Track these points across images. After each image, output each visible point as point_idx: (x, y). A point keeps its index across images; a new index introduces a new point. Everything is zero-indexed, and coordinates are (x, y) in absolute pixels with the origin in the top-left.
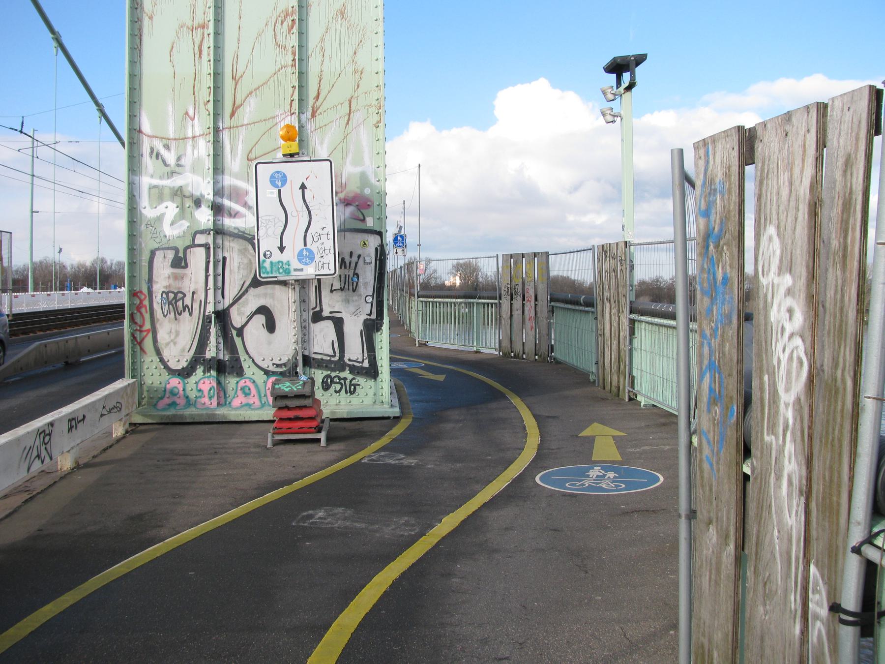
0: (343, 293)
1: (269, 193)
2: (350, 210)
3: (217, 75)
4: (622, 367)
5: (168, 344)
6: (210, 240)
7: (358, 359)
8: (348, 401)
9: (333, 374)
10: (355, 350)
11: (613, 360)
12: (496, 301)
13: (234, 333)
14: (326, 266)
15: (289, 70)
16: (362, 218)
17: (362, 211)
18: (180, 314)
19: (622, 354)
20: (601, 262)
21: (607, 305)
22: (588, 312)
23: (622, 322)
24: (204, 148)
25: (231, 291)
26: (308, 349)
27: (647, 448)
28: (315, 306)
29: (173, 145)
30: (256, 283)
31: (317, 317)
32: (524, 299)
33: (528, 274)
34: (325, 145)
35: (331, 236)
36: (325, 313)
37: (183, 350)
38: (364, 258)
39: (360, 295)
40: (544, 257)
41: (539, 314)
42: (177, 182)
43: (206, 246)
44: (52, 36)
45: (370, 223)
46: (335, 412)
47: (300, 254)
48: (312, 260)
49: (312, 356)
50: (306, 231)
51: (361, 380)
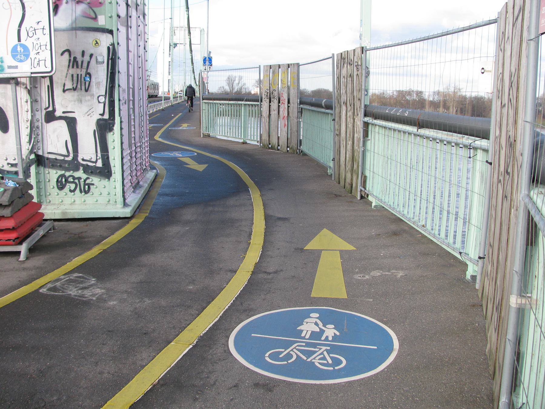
0: (76, 93)
4: (355, 166)
7: (91, 159)
8: (83, 200)
11: (347, 159)
12: (258, 103)
14: (42, 63)
16: (94, 16)
17: (95, 9)
19: (355, 154)
20: (339, 68)
21: (344, 108)
22: (328, 114)
23: (357, 125)
26: (41, 149)
27: (377, 273)
28: (47, 106)
31: (50, 117)
32: (279, 102)
33: (282, 82)
35: (47, 31)
36: (58, 113)
38: (96, 57)
39: (93, 95)
40: (296, 67)
41: (290, 115)
45: (102, 21)
46: (66, 212)
47: (14, 49)
48: (27, 56)
49: (46, 155)
50: (20, 25)
51: (95, 180)
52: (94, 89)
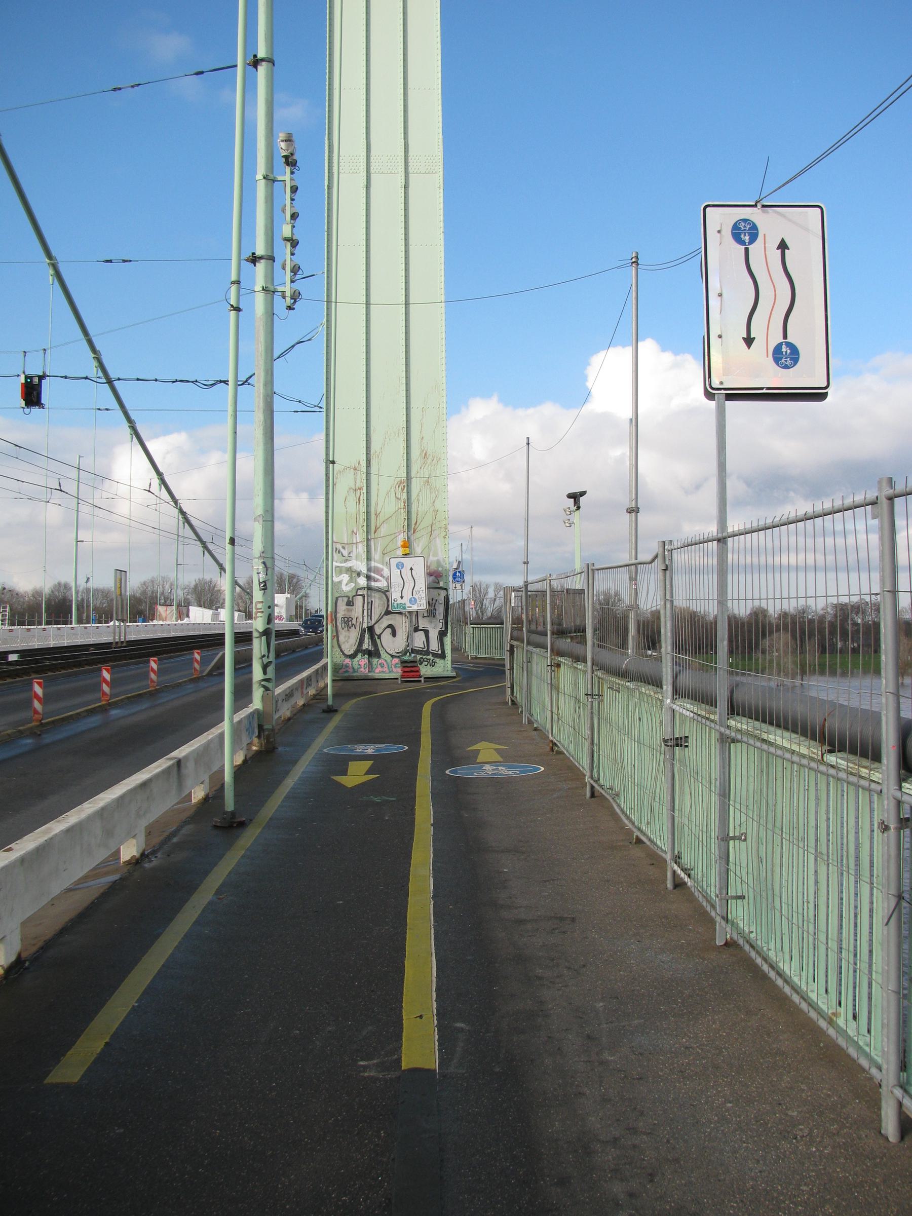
0: (428, 618)
1: (395, 572)
2: (432, 578)
3: (368, 513)
5: (344, 643)
6: (365, 592)
9: (424, 657)
10: (434, 646)
13: (376, 637)
15: (402, 510)
18: (350, 628)
24: (362, 549)
25: (375, 617)
29: (346, 546)
30: (388, 613)
31: (416, 629)
32: (537, 624)
34: (420, 547)
36: (420, 628)
37: (352, 645)
42: (348, 564)
43: (363, 596)
44: (93, 355)
45: (441, 584)
48: (416, 602)
51: (437, 660)
52: (437, 616)
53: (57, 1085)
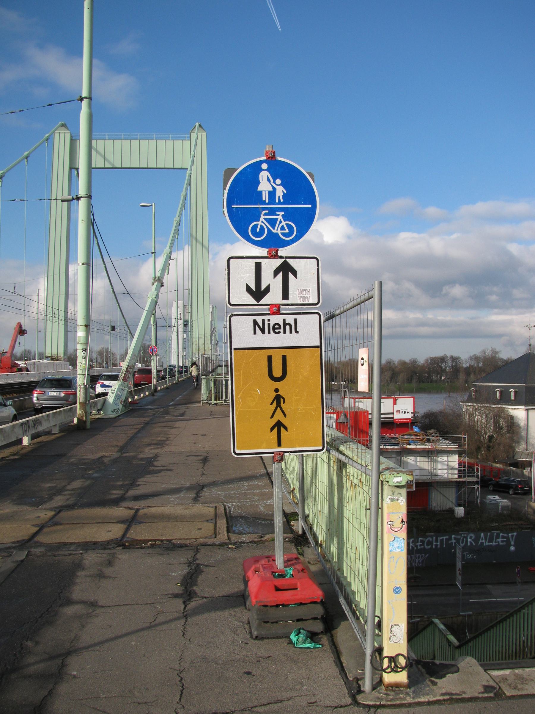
53: (275, 428)
